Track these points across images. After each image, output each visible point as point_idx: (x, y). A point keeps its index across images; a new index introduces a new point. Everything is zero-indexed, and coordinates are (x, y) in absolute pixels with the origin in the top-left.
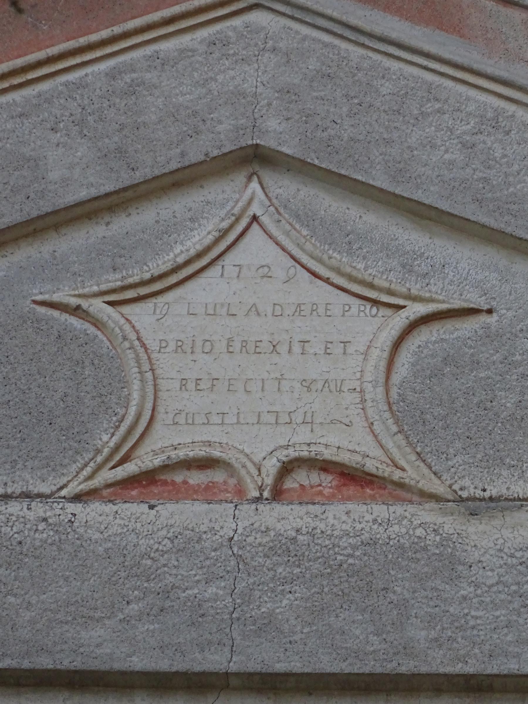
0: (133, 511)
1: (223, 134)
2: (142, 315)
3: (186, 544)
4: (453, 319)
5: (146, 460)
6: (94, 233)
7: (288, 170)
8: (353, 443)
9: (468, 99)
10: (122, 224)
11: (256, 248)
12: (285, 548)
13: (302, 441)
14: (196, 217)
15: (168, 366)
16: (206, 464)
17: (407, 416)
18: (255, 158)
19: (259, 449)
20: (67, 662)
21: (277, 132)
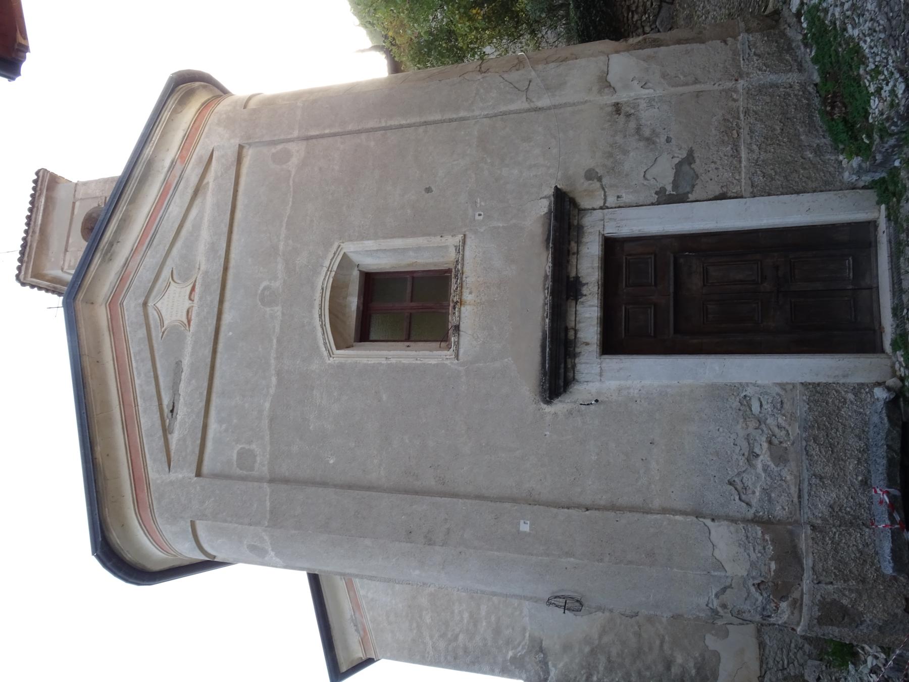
0: (192, 323)
1: (140, 309)
2: (166, 323)
3: (198, 314)
4: (806, 355)
5: (186, 322)
6: (153, 330)
7: (410, 607)
8: (189, 288)
9: (740, 173)
10: (152, 326)
11: (159, 305)
12: (200, 299)
13: (187, 297)
14: (152, 313)
15: (174, 318)
16: (188, 312)
17: (185, 280)
18: (145, 304)
19: (188, 304)
20: (213, 333)
21: (141, 301)
